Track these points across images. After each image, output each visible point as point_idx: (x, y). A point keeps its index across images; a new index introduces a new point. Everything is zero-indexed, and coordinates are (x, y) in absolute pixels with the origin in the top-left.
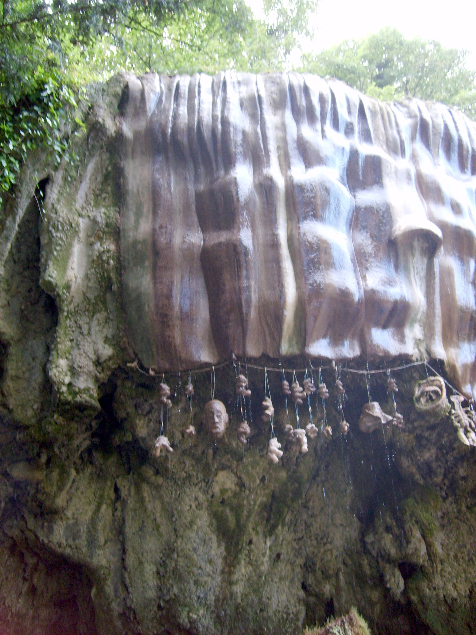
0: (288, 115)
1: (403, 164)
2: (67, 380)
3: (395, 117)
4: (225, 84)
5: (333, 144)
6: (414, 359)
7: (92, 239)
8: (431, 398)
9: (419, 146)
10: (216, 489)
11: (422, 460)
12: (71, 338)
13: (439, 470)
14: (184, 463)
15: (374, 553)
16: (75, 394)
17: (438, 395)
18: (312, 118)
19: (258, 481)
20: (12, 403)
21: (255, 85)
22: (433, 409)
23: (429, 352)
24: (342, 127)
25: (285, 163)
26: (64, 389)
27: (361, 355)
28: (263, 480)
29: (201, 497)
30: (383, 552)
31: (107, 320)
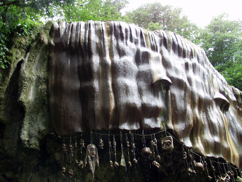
0: (113, 37)
1: (158, 54)
2: (27, 139)
3: (154, 37)
4: (90, 25)
5: (130, 47)
7: (38, 84)
8: (167, 144)
9: (163, 48)
11: (167, 166)
12: (29, 123)
13: (174, 170)
16: (30, 145)
17: (171, 143)
18: (122, 39)
19: (103, 177)
20: (6, 148)
21: (101, 25)
23: (167, 127)
24: (134, 41)
25: (112, 56)
26: (26, 143)
28: (105, 176)
31: (43, 116)
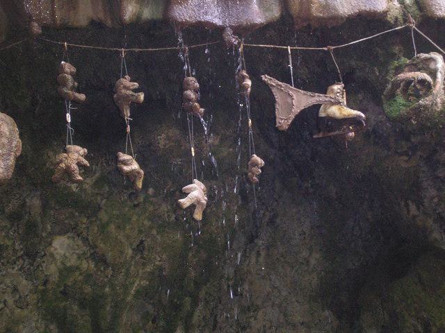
6: (390, 18)
10: (52, 270)
27: (282, 17)
28: (140, 248)
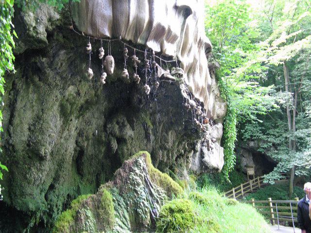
14: (56, 78)
15: (108, 132)
22: (177, 81)
29: (59, 96)
30: (113, 133)
